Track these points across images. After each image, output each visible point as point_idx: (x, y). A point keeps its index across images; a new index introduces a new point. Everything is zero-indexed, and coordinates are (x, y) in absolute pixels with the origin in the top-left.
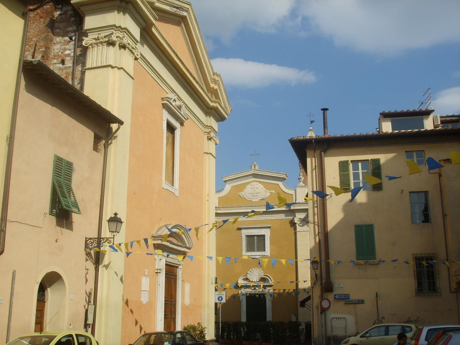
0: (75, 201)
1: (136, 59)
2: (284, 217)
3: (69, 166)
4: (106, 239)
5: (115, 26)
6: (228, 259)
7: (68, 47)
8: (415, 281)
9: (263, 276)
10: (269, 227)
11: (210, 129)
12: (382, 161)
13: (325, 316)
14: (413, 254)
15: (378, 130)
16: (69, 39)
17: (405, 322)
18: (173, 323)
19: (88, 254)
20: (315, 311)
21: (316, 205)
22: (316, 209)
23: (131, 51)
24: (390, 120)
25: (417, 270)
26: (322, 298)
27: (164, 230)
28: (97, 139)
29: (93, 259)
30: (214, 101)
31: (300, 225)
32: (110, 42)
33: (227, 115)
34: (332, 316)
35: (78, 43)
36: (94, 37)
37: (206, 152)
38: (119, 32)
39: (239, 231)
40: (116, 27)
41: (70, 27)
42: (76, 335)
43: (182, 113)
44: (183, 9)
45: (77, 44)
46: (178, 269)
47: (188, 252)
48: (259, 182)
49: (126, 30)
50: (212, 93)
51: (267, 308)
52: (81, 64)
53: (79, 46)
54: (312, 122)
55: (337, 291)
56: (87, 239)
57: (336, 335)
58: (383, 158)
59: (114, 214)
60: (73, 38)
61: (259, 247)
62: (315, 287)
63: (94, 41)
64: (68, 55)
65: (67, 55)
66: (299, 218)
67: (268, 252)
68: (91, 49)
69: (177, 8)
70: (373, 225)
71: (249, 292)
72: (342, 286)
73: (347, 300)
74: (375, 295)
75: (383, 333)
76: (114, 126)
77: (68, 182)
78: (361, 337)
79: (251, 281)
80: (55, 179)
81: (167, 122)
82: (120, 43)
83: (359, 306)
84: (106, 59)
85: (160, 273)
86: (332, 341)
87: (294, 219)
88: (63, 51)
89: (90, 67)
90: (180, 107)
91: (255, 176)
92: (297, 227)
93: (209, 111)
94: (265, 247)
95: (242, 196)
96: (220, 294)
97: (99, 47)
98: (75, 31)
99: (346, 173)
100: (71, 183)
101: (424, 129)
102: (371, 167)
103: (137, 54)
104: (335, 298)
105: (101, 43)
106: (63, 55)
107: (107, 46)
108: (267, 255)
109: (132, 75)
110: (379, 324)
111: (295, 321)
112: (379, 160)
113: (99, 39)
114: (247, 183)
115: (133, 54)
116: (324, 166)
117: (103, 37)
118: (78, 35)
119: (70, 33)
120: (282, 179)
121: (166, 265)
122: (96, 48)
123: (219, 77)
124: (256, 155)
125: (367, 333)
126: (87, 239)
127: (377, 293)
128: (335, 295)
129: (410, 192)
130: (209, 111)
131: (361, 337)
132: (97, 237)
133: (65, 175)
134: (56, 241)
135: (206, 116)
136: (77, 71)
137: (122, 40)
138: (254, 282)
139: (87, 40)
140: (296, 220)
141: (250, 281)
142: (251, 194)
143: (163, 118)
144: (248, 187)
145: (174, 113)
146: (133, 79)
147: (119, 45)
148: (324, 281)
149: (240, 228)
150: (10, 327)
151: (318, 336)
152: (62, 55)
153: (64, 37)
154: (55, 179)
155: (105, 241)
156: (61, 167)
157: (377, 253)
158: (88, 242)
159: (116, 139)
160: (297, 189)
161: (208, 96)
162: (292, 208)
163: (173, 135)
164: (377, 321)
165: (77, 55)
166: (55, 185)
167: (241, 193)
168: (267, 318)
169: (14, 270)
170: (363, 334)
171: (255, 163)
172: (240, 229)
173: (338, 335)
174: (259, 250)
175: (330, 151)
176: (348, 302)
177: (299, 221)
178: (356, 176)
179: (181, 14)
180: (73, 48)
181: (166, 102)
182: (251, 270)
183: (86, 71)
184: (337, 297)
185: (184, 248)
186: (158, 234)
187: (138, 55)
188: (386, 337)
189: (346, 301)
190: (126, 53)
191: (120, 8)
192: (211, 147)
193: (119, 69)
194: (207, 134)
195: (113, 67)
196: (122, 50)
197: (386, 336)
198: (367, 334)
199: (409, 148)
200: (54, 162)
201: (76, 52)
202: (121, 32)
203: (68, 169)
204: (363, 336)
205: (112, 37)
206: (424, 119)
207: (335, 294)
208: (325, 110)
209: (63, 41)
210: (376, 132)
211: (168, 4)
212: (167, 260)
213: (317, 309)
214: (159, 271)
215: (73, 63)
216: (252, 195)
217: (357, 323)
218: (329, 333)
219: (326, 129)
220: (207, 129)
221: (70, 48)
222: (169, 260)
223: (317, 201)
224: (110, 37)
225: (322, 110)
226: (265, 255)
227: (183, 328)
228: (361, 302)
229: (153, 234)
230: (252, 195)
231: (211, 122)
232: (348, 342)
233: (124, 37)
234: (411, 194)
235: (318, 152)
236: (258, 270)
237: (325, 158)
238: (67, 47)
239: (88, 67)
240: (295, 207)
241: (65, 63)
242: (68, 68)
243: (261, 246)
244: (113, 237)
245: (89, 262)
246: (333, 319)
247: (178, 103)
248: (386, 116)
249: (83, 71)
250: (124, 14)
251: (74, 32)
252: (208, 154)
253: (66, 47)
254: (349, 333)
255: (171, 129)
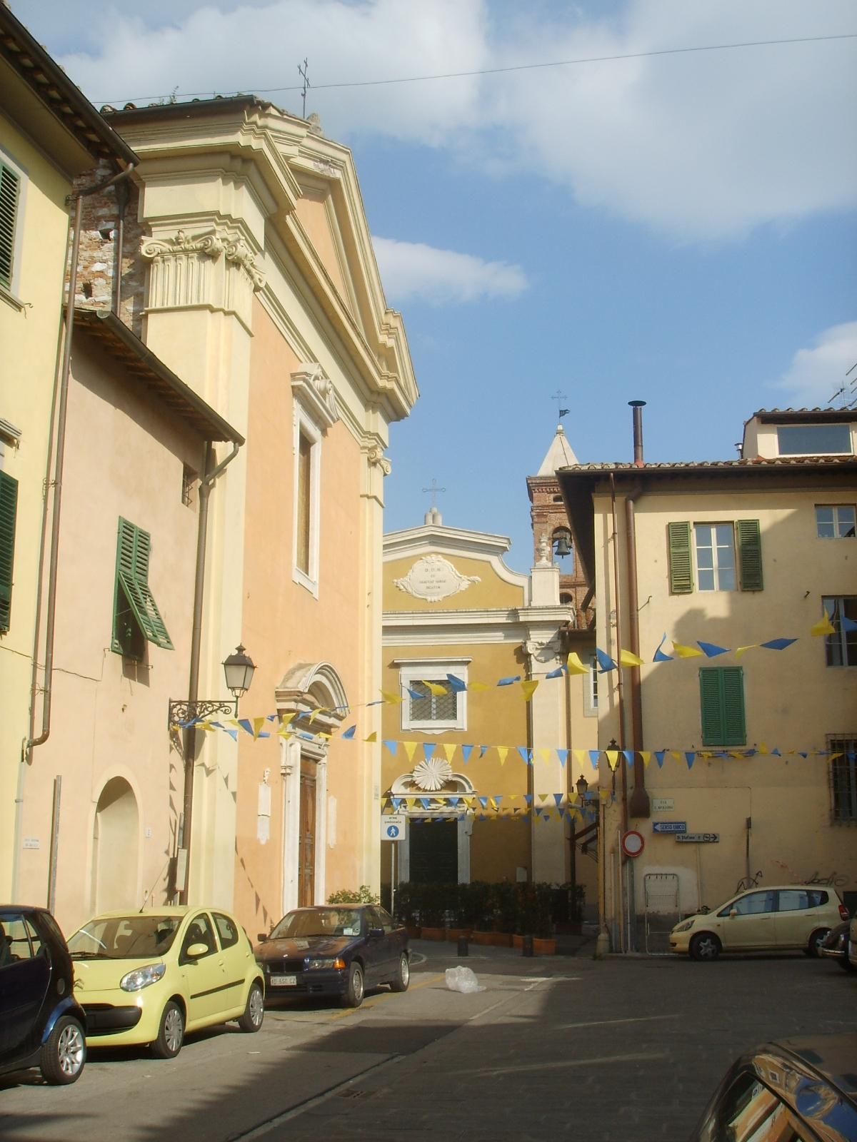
0: (158, 621)
1: (257, 289)
2: (503, 638)
3: (144, 537)
4: (218, 704)
5: (217, 213)
6: (467, 748)
7: (100, 256)
8: (830, 792)
9: (450, 778)
10: (467, 663)
11: (375, 439)
12: (763, 526)
13: (632, 870)
14: (827, 735)
15: (740, 447)
16: (100, 235)
17: (805, 883)
18: (309, 886)
19: (174, 735)
20: (610, 860)
21: (614, 621)
22: (614, 630)
23: (249, 272)
24: (776, 430)
25: (835, 769)
26: (626, 831)
27: (301, 679)
28: (189, 475)
29: (181, 748)
30: (388, 376)
31: (539, 658)
32: (207, 251)
33: (410, 406)
34: (648, 870)
35: (123, 246)
36: (167, 237)
37: (365, 494)
38: (226, 228)
39: (394, 670)
40: (221, 217)
41: (102, 207)
42: (213, 914)
43: (327, 405)
44: (335, 164)
45: (123, 250)
46: (318, 766)
47: (338, 727)
48: (445, 555)
49: (240, 224)
50: (379, 356)
51: (459, 851)
52: (132, 298)
53: (126, 254)
54: (563, 413)
55: (658, 815)
56: (172, 704)
57: (656, 912)
58: (767, 517)
59: (237, 649)
60: (112, 235)
61: (441, 710)
62: (609, 806)
63: (168, 247)
64: (101, 274)
65: (98, 274)
66: (538, 643)
67: (462, 721)
68: (161, 265)
69: (326, 162)
70: (741, 668)
71: (417, 814)
72: (669, 803)
73: (680, 835)
74: (744, 822)
75: (762, 906)
76: (221, 449)
77: (142, 577)
78: (719, 915)
79: (422, 787)
80: (121, 572)
81: (301, 433)
82: (230, 255)
83: (707, 848)
84: (199, 292)
85: (289, 774)
86: (647, 926)
87: (525, 643)
88: (86, 264)
89: (159, 306)
90: (324, 393)
91: (435, 540)
92: (533, 663)
93: (378, 400)
94: (455, 709)
95: (402, 587)
96: (392, 820)
97: (179, 262)
98: (116, 219)
99: (682, 550)
100: (147, 579)
101: (851, 452)
102: (738, 539)
103: (259, 279)
104: (655, 830)
105: (185, 251)
106: (89, 273)
107: (199, 261)
108: (461, 727)
109: (249, 325)
110: (750, 887)
111: (523, 883)
112: (756, 523)
113: (179, 244)
114: (414, 556)
115: (252, 277)
116: (633, 534)
117: (189, 237)
118: (125, 227)
119: (104, 223)
120: (499, 551)
121: (303, 757)
122: (172, 263)
123: (398, 319)
124: (437, 490)
125: (731, 906)
126: (172, 704)
127: (749, 821)
128: (655, 824)
129: (823, 597)
130: (374, 398)
131: (719, 915)
132: (187, 699)
133: (138, 562)
134: (123, 710)
135: (367, 410)
136: (124, 314)
137: (234, 248)
138: (430, 791)
139: (149, 243)
140: (531, 648)
141: (419, 789)
142: (425, 582)
143: (293, 421)
144: (418, 566)
145: (313, 408)
146: (251, 335)
147: (226, 259)
148: (630, 792)
149: (397, 664)
150: (54, 899)
151: (615, 916)
152: (85, 273)
153: (89, 230)
154: (121, 572)
155: (215, 708)
156: (131, 544)
157: (748, 732)
158: (175, 711)
159: (223, 476)
160: (533, 575)
161: (373, 362)
162: (522, 619)
163: (306, 456)
164: (745, 881)
165: (123, 275)
166: (123, 587)
167: (400, 582)
168: (459, 875)
169: (58, 776)
170: (724, 910)
171: (435, 510)
172: (396, 666)
173: (658, 912)
174: (441, 716)
175: (648, 500)
176: (684, 840)
177: (537, 649)
178: (705, 557)
179: (331, 176)
180: (113, 258)
181: (301, 383)
182: (422, 763)
183: (149, 315)
184: (658, 827)
185: (333, 718)
186: (287, 688)
187: (261, 281)
188: (772, 915)
189: (679, 837)
190: (239, 276)
191: (228, 173)
192: (375, 482)
193: (227, 313)
194: (367, 451)
195: (213, 310)
196: (233, 269)
197: (773, 913)
198: (732, 909)
199: (824, 497)
200: (119, 533)
201: (120, 267)
202: (229, 228)
203: (142, 548)
204: (723, 913)
205: (212, 240)
206: (850, 429)
207: (656, 821)
208: (637, 404)
209: (87, 240)
210: (733, 457)
211: (312, 156)
212: (304, 747)
213: (614, 856)
214: (288, 771)
215: (114, 293)
216: (428, 585)
217: (701, 886)
218: (640, 908)
219: (640, 448)
220: (366, 439)
221: (104, 258)
222: (308, 746)
223: (617, 611)
224: (207, 239)
225: (630, 403)
226: (455, 728)
227: (329, 898)
228: (712, 840)
229: (277, 688)
230: (428, 585)
231: (376, 422)
232: (690, 927)
233: (238, 240)
234: (826, 601)
235: (620, 500)
236: (440, 761)
237: (635, 514)
238: (97, 254)
239: (153, 307)
240: (530, 617)
241: (93, 293)
242: (102, 305)
243: (445, 707)
244: (235, 699)
245: (175, 752)
246: (648, 877)
247: (319, 385)
248: (767, 419)
249: (142, 315)
250: (237, 187)
251: (113, 221)
252: (368, 497)
253: (95, 255)
254: (685, 906)
255: (306, 444)
